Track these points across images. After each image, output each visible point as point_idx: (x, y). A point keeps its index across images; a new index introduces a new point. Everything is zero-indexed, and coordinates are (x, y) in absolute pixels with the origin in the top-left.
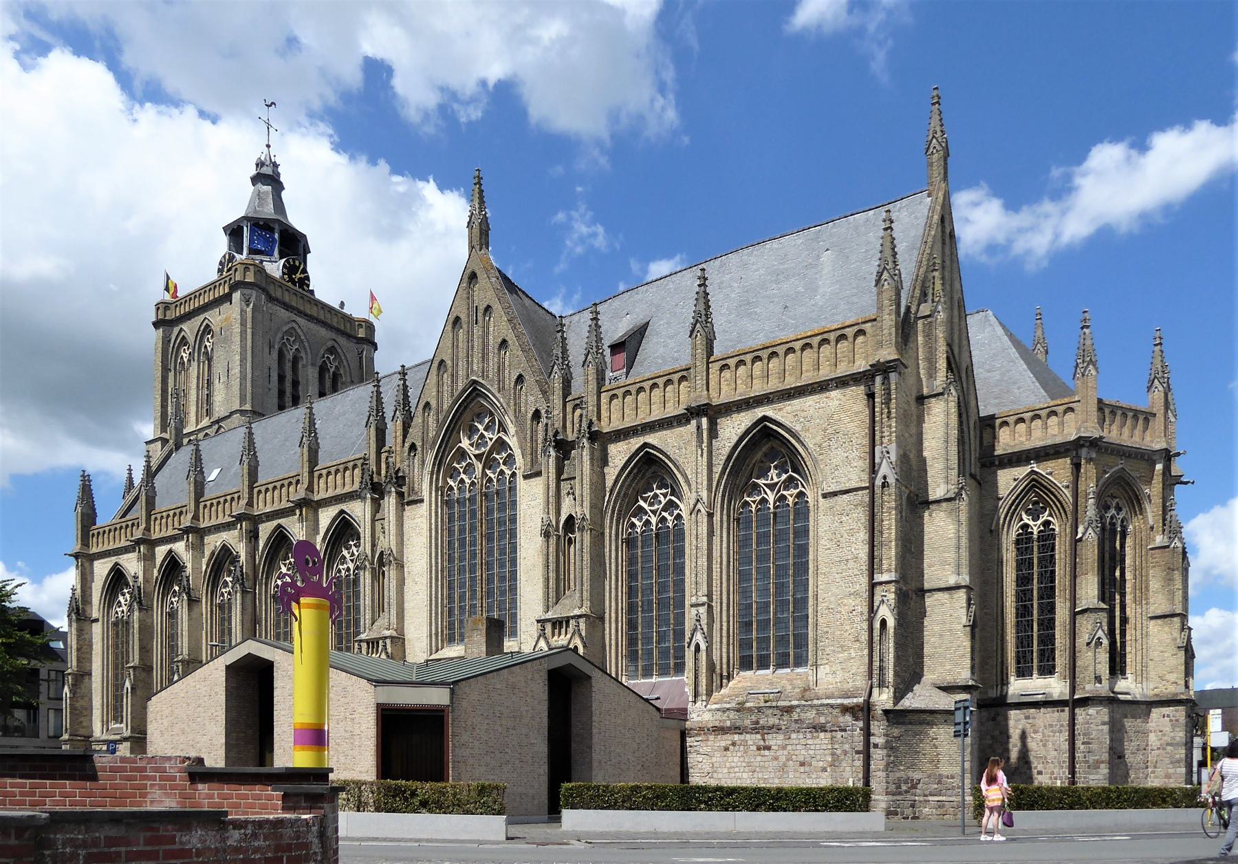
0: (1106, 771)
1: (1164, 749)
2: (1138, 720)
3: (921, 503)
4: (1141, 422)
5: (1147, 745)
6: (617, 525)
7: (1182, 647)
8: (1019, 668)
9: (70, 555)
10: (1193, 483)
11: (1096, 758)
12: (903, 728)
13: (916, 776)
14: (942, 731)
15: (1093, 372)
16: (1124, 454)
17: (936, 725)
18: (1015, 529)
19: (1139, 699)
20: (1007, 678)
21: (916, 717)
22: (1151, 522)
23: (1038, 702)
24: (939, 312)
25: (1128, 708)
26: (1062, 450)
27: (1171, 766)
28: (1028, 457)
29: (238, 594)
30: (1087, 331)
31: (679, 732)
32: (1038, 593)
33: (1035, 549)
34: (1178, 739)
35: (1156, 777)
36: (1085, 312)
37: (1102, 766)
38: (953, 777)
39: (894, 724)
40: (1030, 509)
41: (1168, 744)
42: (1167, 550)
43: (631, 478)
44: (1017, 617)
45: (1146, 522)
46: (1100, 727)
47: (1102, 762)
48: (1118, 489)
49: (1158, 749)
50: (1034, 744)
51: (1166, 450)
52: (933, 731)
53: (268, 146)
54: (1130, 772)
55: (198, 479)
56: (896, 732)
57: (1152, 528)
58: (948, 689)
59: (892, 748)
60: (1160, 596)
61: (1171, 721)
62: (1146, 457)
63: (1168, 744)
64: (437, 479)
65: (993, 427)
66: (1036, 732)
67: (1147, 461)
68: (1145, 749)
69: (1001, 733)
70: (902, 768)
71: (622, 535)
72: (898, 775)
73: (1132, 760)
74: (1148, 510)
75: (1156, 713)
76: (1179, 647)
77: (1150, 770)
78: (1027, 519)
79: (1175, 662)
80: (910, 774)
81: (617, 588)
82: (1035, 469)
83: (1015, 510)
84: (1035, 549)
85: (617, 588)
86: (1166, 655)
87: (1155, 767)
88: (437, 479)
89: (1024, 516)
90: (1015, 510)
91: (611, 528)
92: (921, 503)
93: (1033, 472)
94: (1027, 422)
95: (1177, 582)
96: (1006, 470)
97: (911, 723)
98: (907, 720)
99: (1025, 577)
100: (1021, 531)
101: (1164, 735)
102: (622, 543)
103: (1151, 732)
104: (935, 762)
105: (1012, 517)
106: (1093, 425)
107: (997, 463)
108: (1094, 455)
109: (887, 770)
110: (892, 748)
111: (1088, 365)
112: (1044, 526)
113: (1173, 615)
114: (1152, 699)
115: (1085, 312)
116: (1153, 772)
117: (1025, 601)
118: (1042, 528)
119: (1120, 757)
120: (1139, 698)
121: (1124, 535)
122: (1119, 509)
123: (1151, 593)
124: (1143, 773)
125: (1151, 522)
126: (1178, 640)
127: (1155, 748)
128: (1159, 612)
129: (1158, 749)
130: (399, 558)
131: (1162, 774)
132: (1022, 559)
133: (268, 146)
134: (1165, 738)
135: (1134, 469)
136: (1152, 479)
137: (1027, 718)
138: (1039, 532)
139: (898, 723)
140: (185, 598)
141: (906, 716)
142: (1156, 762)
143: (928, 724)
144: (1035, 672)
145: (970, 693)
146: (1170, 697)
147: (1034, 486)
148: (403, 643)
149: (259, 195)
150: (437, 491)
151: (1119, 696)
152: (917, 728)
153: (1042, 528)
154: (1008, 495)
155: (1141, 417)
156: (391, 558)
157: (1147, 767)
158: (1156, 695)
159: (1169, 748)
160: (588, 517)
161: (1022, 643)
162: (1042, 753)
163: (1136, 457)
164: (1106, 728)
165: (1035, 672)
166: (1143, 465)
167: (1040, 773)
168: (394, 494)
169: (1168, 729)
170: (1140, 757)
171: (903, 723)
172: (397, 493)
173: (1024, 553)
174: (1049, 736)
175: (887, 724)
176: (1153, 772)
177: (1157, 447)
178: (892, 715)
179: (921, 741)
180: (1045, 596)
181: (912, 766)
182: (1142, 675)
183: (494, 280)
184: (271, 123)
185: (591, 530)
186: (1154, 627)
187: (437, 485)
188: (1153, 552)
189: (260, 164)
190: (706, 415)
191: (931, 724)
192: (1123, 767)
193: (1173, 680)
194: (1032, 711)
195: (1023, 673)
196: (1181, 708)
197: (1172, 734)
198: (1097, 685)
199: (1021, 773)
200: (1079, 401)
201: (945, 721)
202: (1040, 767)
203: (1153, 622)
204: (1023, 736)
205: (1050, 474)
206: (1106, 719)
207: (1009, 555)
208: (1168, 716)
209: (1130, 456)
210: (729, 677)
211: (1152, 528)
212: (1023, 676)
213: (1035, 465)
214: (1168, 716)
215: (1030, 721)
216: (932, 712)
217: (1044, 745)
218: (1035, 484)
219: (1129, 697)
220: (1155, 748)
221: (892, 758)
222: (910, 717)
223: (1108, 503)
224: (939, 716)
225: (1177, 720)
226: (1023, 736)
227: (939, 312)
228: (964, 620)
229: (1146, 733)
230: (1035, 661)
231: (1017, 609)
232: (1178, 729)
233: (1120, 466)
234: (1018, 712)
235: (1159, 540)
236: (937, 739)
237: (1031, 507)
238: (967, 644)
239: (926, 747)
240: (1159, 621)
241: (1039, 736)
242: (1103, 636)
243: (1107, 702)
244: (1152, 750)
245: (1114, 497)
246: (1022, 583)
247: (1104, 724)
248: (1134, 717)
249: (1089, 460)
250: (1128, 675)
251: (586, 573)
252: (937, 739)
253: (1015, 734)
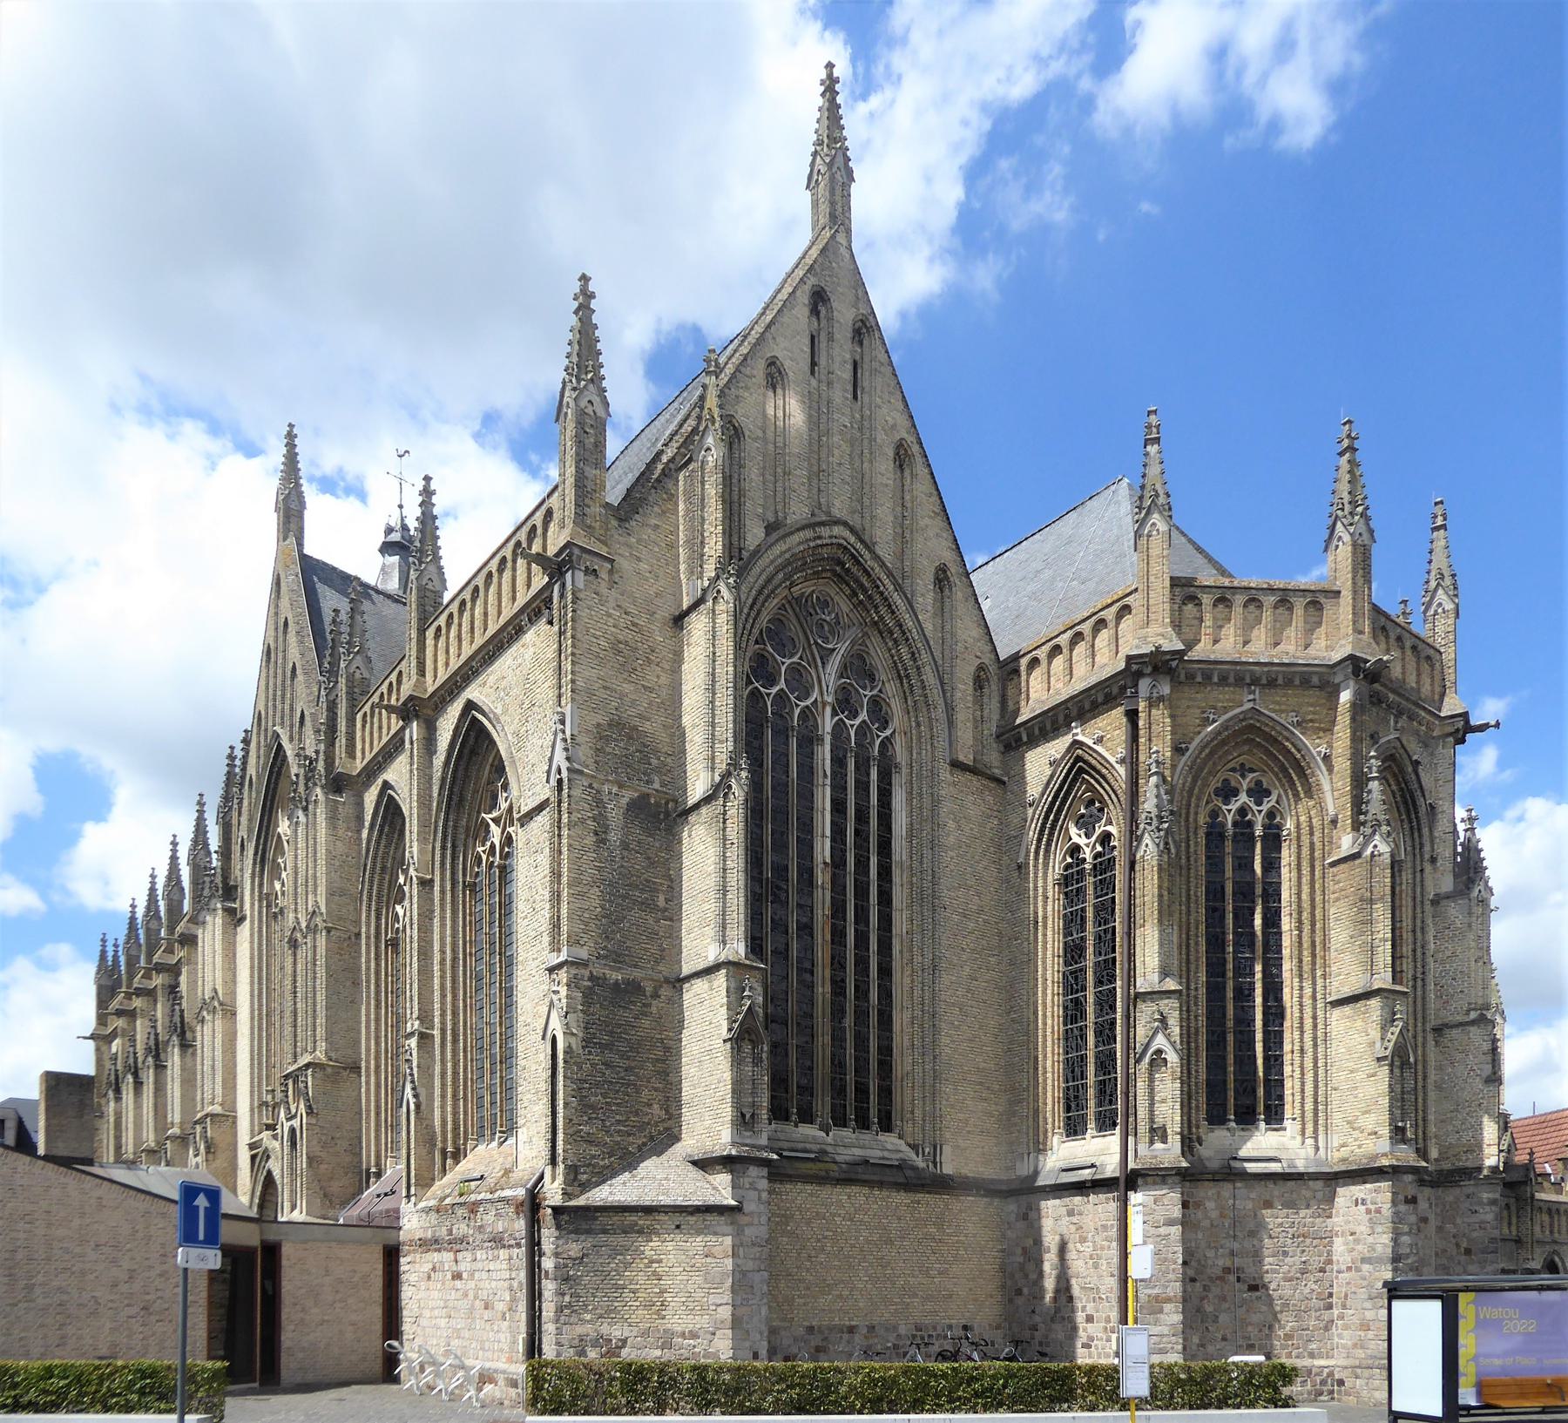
0: (1178, 1318)
1: (1358, 1270)
2: (1303, 1213)
3: (680, 815)
4: (1299, 611)
5: (1330, 1262)
6: (378, 918)
7: (1385, 1058)
8: (1069, 1118)
9: (85, 1038)
10: (1497, 725)
11: (1156, 1291)
12: (589, 1242)
13: (616, 1332)
14: (670, 1246)
15: (1162, 526)
16: (1255, 681)
17: (658, 1234)
18: (1059, 857)
19: (1302, 1170)
20: (1046, 1137)
21: (632, 1218)
22: (1331, 811)
23: (1084, 1182)
24: (708, 449)
25: (1275, 1190)
26: (1115, 690)
27: (1368, 1305)
28: (1066, 716)
29: (151, 1071)
30: (1153, 449)
31: (379, 1249)
32: (1095, 973)
33: (1090, 891)
34: (1379, 1249)
35: (1346, 1327)
36: (1150, 413)
37: (1168, 1307)
38: (694, 1335)
39: (572, 1232)
40: (1083, 816)
41: (1364, 1260)
42: (1358, 862)
43: (383, 842)
44: (1065, 1024)
45: (1322, 810)
46: (1163, 1230)
47: (1169, 1300)
48: (1249, 752)
49: (1349, 1269)
50: (1080, 1263)
51: (1351, 657)
52: (651, 1247)
53: (401, 507)
54: (1283, 1317)
55: (150, 925)
56: (574, 1249)
57: (1334, 822)
58: (704, 1164)
59: (567, 1279)
60: (1347, 957)
61: (1368, 1211)
62: (1315, 680)
63: (1364, 1260)
64: (261, 885)
65: (1017, 672)
66: (1083, 1240)
67: (1320, 688)
68: (1322, 1270)
69: (1035, 1244)
70: (588, 1317)
71: (386, 935)
72: (580, 1330)
73: (1287, 1292)
74: (1326, 786)
75: (1346, 1195)
76: (1379, 1059)
77: (1336, 1312)
78: (1076, 836)
79: (1372, 1091)
80: (605, 1329)
81: (377, 1020)
82: (1080, 738)
83: (1056, 820)
84: (1090, 891)
85: (377, 1020)
86: (1361, 1075)
87: (1344, 1307)
88: (261, 885)
89: (1073, 830)
90: (1056, 820)
91: (368, 925)
92: (680, 815)
93: (1075, 742)
94: (1064, 650)
95: (1380, 926)
96: (1039, 749)
97: (605, 1232)
98: (597, 1225)
99: (1076, 946)
100: (1069, 860)
101: (1357, 1241)
102: (386, 947)
103: (1337, 1235)
104: (658, 1307)
105: (1051, 834)
106: (1161, 630)
107: (1025, 739)
108: (1166, 689)
109: (557, 1321)
110: (567, 1279)
111: (1148, 513)
112: (1102, 844)
113: (1367, 995)
114: (1336, 1169)
115: (1150, 413)
116: (1341, 1317)
117: (1077, 992)
118: (1099, 848)
119: (1254, 1288)
120: (1301, 1166)
121: (1273, 840)
122: (1259, 793)
123: (1333, 954)
124: (1318, 1319)
125: (1331, 811)
126: (1378, 1045)
127: (1344, 1267)
128: (1346, 991)
129: (1349, 1269)
130: (227, 1001)
131: (1356, 1320)
132: (1071, 912)
133: (401, 507)
134: (1360, 1247)
135: (1279, 710)
136: (1333, 722)
137: (1071, 1213)
138: (1095, 857)
139: (577, 1232)
140: (131, 1080)
141: (596, 1219)
142: (1346, 1295)
143: (640, 1232)
144: (1091, 1125)
145: (731, 1172)
146: (1364, 1163)
147: (1081, 770)
148: (234, 1123)
149: (382, 569)
150: (260, 901)
151: (1246, 1165)
152: (620, 1240)
153: (1099, 848)
154: (1043, 795)
155: (1299, 604)
156: (216, 1004)
157: (1330, 1307)
158: (1344, 1160)
159: (1366, 1267)
160: (323, 910)
161: (1073, 1072)
162: (1093, 1281)
163: (1289, 683)
164: (1176, 1231)
165: (1091, 1125)
166: (1312, 696)
167: (1090, 1319)
168: (220, 912)
169: (1363, 1229)
170: (1310, 1286)
171: (588, 1232)
172: (225, 910)
173: (1075, 899)
174: (1102, 1248)
175: (556, 1233)
176: (1341, 1317)
177: (1337, 656)
178: (566, 1217)
179: (627, 1265)
180: (1105, 980)
181: (609, 1314)
182: (1316, 1121)
183: (1198, 696)
184: (405, 476)
185: (329, 930)
186: (1339, 1019)
187: (260, 892)
188: (1334, 870)
189: (389, 530)
190: (417, 717)
191: (647, 1233)
192: (1264, 1308)
193: (1370, 1128)
194: (1078, 1199)
195: (1074, 1129)
196: (1385, 1185)
197: (1370, 1239)
198: (1158, 1146)
199: (1063, 1319)
200: (1136, 590)
201: (678, 1227)
202: (1090, 1309)
203: (1337, 1013)
204: (1063, 1248)
205: (1100, 740)
206: (1177, 1212)
207: (1048, 906)
208: (1364, 1202)
209: (1272, 683)
210: (457, 1155)
211: (1334, 822)
212: (1075, 1133)
213: (1079, 730)
214: (1364, 1202)
215: (1074, 1219)
216: (649, 1210)
217: (1096, 1266)
218: (1080, 767)
219: (1274, 1167)
220: (1344, 1267)
221: (567, 1298)
222: (603, 1219)
223: (1233, 784)
224: (662, 1217)
225: (1378, 1211)
226: (1063, 1248)
227: (708, 449)
228: (725, 1034)
229: (1327, 1238)
230: (1092, 1103)
231: (1066, 1008)
232: (1379, 1229)
233: (1250, 705)
234: (1057, 1202)
235: (1346, 843)
236: (660, 1261)
237: (1083, 811)
238: (728, 1076)
239: (638, 1277)
240: (1347, 1010)
241: (1087, 1248)
242: (1167, 1048)
243: (1177, 1179)
244: (1339, 1272)
245: (1243, 770)
246: (1073, 957)
247: (1170, 1223)
248: (1291, 1205)
249: (1152, 703)
250: (1287, 1123)
251: (321, 997)
252: (660, 1261)
253: (1050, 1240)
